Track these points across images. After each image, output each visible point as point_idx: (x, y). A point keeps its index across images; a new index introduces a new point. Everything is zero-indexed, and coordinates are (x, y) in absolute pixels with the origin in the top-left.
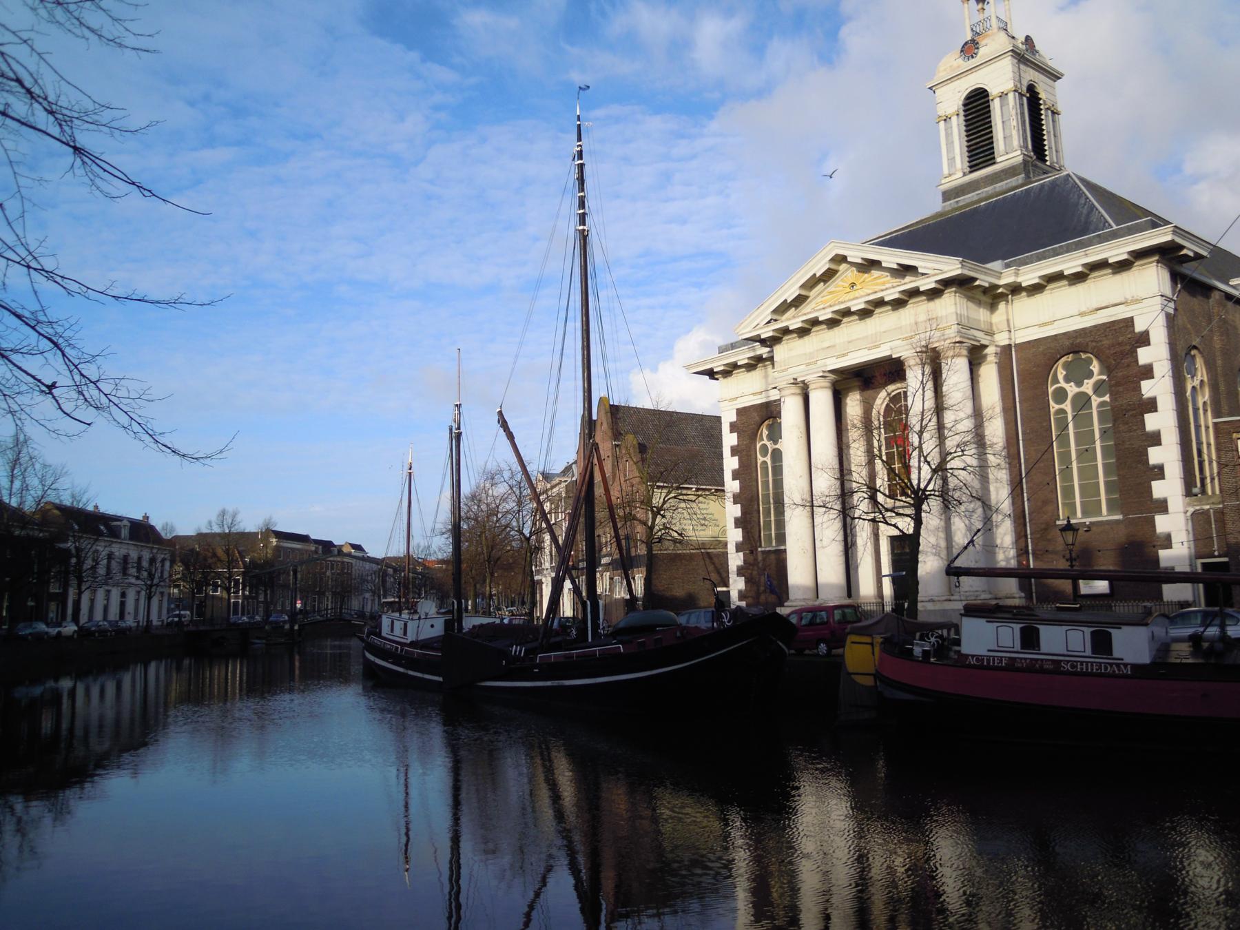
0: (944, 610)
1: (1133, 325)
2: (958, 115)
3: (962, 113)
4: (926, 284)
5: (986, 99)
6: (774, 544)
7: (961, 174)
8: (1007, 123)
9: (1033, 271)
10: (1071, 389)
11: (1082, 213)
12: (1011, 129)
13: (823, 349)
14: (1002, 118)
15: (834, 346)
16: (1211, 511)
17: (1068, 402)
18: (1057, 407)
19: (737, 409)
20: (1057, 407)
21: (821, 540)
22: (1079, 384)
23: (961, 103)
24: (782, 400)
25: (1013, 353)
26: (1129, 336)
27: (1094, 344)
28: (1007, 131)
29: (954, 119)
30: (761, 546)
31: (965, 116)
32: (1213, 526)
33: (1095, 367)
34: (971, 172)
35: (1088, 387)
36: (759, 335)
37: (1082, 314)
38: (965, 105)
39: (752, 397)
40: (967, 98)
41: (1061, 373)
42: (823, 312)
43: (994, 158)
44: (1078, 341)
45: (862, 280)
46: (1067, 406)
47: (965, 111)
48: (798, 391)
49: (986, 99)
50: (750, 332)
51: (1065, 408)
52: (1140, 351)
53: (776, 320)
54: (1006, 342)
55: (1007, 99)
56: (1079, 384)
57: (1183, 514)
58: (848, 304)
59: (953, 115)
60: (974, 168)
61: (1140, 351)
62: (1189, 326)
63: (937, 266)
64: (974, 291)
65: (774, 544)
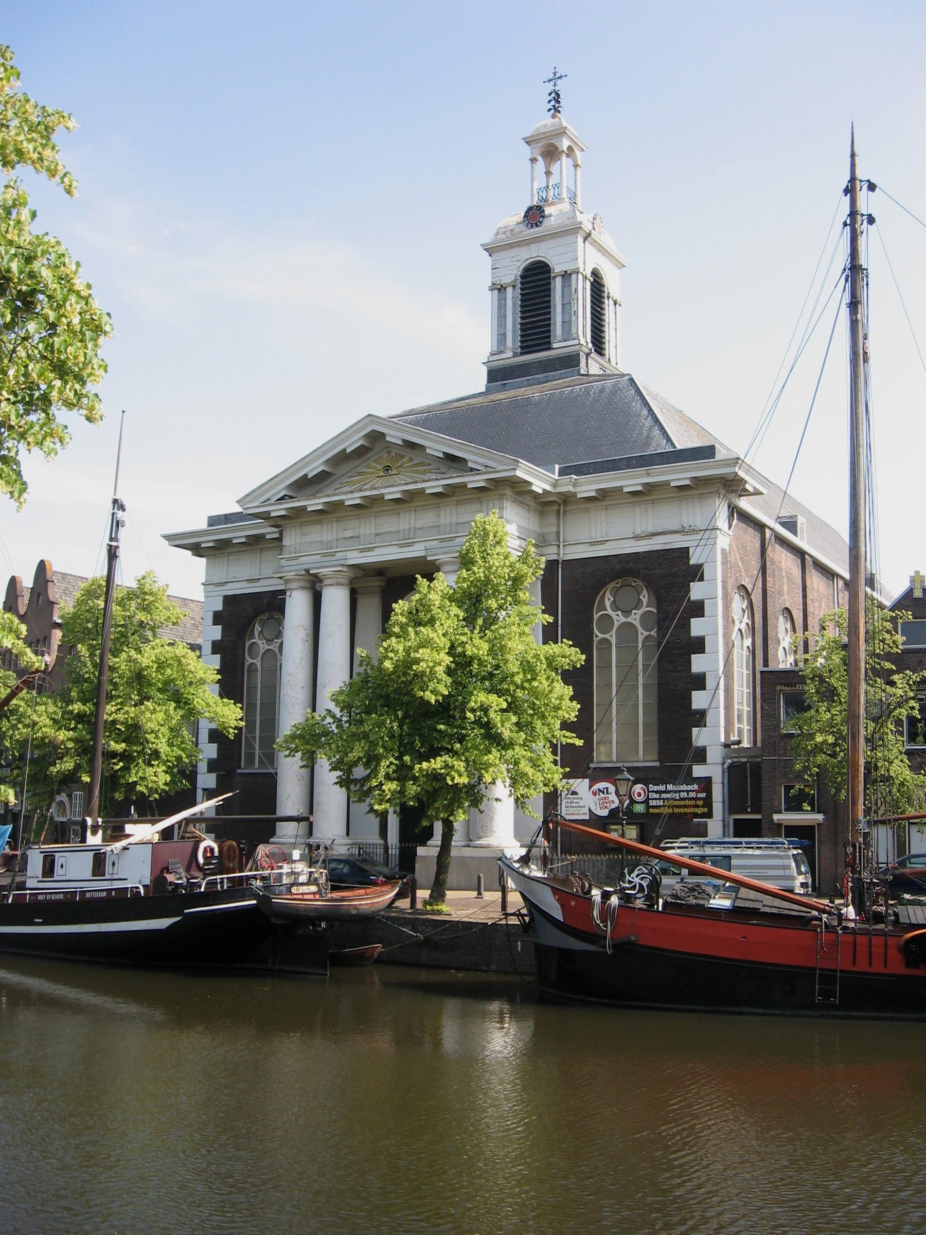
0: (462, 857)
1: (688, 558)
2: (514, 286)
3: (519, 286)
4: (475, 481)
5: (548, 275)
6: (257, 765)
7: (511, 354)
8: (568, 306)
9: (591, 483)
10: (618, 618)
11: (644, 424)
12: (570, 313)
13: (344, 538)
14: (563, 300)
15: (358, 537)
16: (748, 764)
17: (613, 632)
18: (601, 636)
19: (225, 597)
20: (601, 636)
21: (114, 864)
22: (627, 613)
23: (519, 273)
24: (288, 594)
25: (560, 569)
26: (683, 568)
27: (646, 571)
28: (567, 315)
29: (509, 290)
30: (239, 767)
31: (522, 289)
32: (749, 781)
33: (645, 598)
34: (522, 354)
35: (635, 618)
36: (269, 512)
37: (637, 538)
38: (522, 277)
39: (245, 584)
40: (526, 270)
41: (608, 601)
42: (351, 496)
43: (549, 343)
44: (631, 565)
45: (399, 464)
46: (612, 637)
47: (522, 283)
48: (308, 585)
49: (548, 275)
50: (258, 507)
51: (610, 638)
52: (694, 657)
53: (291, 497)
54: (554, 557)
55: (570, 280)
56: (627, 613)
57: (720, 766)
58: (383, 491)
59: (508, 286)
60: (526, 348)
61: (694, 657)
62: (740, 564)
63: (489, 463)
64: (525, 496)
65: (257, 765)
